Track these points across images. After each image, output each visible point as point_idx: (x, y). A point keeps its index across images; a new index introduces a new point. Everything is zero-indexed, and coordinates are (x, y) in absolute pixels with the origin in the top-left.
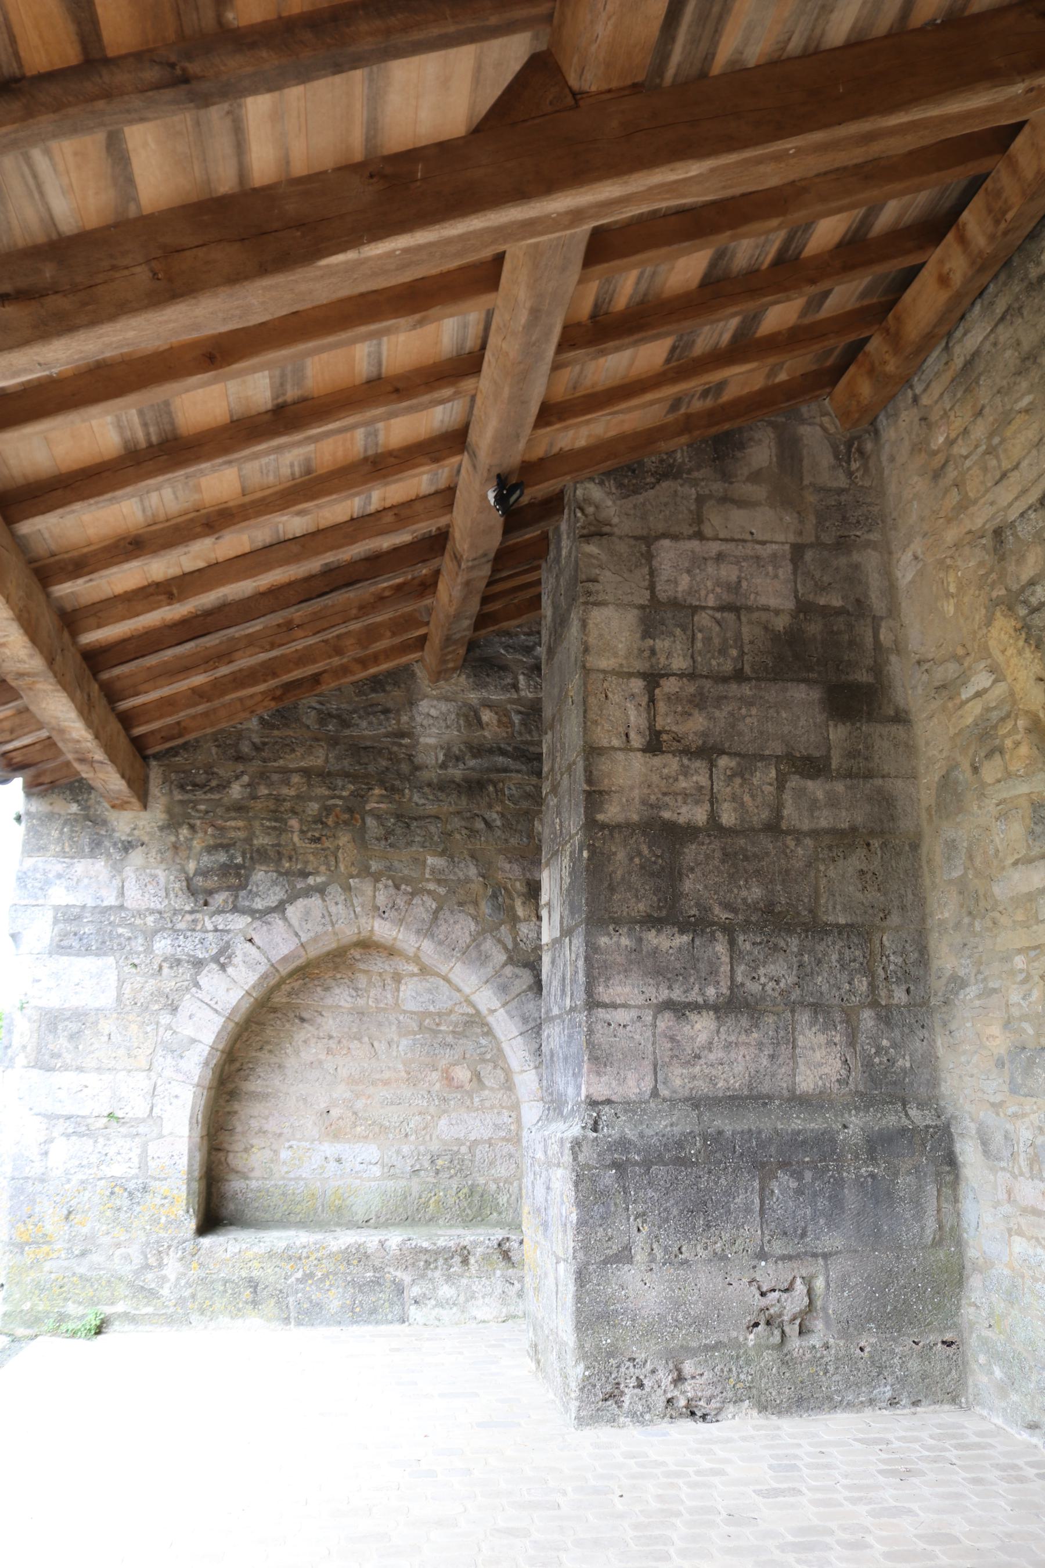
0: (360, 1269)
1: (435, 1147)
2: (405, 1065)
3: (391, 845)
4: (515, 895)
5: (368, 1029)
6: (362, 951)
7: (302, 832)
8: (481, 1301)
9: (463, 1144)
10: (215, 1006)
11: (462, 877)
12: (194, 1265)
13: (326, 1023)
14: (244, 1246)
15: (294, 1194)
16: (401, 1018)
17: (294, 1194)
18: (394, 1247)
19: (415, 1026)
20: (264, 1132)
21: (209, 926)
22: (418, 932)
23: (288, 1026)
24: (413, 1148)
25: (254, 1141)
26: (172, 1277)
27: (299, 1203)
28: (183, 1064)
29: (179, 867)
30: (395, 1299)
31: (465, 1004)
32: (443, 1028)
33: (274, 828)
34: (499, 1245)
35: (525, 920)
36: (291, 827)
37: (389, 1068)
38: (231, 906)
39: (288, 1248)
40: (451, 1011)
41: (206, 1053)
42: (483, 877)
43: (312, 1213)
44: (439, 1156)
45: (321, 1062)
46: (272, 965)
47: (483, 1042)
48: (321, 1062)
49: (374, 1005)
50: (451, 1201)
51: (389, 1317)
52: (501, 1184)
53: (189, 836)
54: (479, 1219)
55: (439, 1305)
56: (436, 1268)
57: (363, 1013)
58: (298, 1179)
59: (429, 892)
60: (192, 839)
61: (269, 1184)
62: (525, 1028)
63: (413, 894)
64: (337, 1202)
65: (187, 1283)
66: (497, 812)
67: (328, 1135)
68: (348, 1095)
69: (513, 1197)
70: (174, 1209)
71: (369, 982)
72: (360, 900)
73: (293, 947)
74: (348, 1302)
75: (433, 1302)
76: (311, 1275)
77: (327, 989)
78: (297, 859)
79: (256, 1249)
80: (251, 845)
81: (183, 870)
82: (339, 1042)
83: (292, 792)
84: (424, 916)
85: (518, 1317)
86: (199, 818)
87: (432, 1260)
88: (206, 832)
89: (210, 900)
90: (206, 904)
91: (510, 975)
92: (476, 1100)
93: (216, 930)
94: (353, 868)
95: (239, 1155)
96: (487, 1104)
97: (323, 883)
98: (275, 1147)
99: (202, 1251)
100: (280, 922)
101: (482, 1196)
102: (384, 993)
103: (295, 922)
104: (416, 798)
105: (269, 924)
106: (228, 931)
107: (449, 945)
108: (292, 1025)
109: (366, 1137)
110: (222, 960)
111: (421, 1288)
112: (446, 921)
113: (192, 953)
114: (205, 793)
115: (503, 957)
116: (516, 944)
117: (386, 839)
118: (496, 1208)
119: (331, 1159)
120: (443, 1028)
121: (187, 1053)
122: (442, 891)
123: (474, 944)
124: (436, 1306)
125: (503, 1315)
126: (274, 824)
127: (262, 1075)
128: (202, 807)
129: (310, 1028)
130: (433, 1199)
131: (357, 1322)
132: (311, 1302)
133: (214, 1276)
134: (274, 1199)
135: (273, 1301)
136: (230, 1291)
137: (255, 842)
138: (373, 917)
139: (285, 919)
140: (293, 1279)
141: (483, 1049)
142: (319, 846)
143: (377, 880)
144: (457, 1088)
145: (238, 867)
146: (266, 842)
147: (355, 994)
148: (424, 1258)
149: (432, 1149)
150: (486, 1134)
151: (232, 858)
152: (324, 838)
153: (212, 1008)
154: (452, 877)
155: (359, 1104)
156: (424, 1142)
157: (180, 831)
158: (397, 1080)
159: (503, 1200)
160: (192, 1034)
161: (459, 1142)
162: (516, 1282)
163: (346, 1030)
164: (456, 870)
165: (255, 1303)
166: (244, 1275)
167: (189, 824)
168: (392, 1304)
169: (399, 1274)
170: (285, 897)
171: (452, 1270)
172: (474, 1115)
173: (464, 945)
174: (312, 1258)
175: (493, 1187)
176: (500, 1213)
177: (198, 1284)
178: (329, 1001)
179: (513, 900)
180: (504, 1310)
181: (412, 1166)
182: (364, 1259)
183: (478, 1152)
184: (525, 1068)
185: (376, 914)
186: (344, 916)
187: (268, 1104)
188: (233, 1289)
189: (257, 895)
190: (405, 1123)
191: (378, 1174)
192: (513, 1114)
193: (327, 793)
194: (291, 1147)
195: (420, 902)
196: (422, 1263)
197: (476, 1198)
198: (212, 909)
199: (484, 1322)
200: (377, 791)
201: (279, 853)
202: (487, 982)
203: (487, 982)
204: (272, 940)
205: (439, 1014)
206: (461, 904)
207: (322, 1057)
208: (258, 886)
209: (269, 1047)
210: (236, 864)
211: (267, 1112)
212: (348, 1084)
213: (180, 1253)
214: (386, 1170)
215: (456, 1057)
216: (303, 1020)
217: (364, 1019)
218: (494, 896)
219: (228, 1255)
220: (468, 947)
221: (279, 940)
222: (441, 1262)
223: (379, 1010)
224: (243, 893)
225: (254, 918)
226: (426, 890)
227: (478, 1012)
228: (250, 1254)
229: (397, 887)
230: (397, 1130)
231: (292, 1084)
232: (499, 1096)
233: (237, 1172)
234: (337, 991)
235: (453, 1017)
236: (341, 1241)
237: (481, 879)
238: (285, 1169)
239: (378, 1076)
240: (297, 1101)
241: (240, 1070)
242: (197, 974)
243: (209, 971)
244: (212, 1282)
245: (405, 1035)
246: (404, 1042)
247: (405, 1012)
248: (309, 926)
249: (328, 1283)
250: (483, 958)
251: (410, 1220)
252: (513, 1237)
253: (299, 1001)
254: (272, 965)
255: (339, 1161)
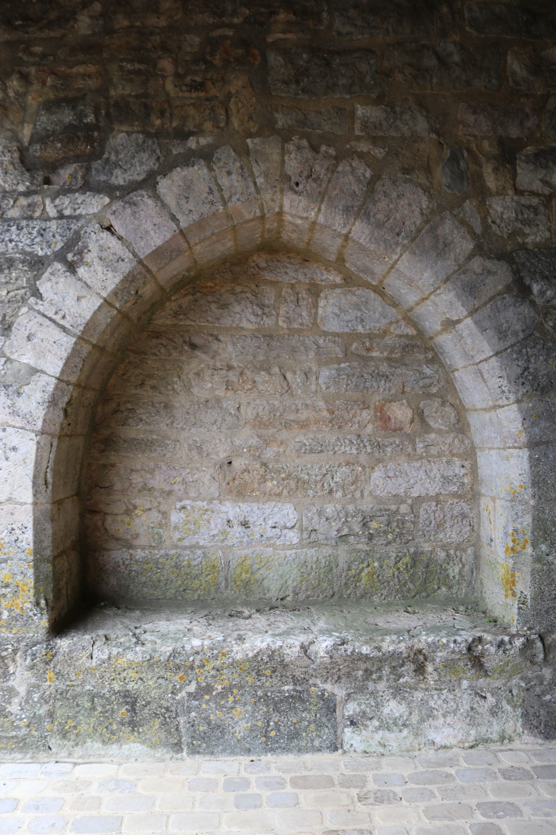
0: (275, 681)
1: (367, 505)
2: (326, 402)
3: (304, 91)
4: (483, 159)
5: (278, 356)
6: (268, 257)
7: (177, 75)
8: (442, 720)
9: (403, 502)
10: (62, 322)
11: (407, 133)
12: (50, 674)
13: (224, 350)
14: (115, 651)
15: (189, 566)
16: (321, 341)
17: (189, 566)
18: (322, 654)
19: (339, 352)
20: (150, 490)
21: (52, 212)
22: (347, 210)
23: (175, 354)
24: (339, 507)
25: (138, 501)
26: (22, 690)
27: (196, 577)
28: (22, 404)
29: (9, 134)
30: (324, 720)
31: (403, 323)
32: (374, 354)
33: (138, 72)
34: (469, 649)
35: (498, 194)
36: (163, 70)
37: (307, 405)
38: (80, 182)
39: (174, 654)
40: (385, 332)
41: (51, 388)
42: (437, 133)
43: (213, 589)
44: (372, 518)
45: (218, 400)
46: (140, 262)
47: (428, 371)
48: (218, 400)
49: (285, 326)
50: (389, 573)
51: (317, 743)
52: (452, 552)
53: (21, 90)
54: (424, 594)
55: (385, 726)
56: (380, 678)
57: (271, 337)
58: (194, 547)
59: (361, 156)
60: (25, 94)
61: (158, 554)
62: (501, 346)
63: (338, 159)
64: (244, 576)
65: (41, 697)
66: (455, 43)
67: (231, 491)
68: (254, 441)
69: (467, 568)
70: (19, 601)
71: (279, 296)
72: (263, 167)
73: (169, 236)
74: (260, 724)
75: (376, 723)
76: (208, 689)
77: (225, 306)
78: (171, 114)
79: (130, 656)
80: (107, 98)
81: (15, 137)
82: (242, 374)
83: (163, 22)
84: (355, 187)
85: (492, 741)
86: (34, 64)
87: (374, 669)
88: (44, 83)
89: (54, 178)
90: (47, 181)
91: (479, 271)
92: (420, 445)
93: (61, 216)
94: (251, 124)
95: (119, 518)
96: (433, 451)
97: (209, 145)
98: (163, 508)
99: (60, 657)
100: (150, 202)
101: (427, 566)
102: (298, 310)
103: (170, 200)
104: (338, 24)
105: (135, 204)
106: (78, 218)
107: (392, 229)
108: (181, 353)
109: (279, 495)
110: (70, 257)
111: (359, 705)
112: (386, 194)
113: (28, 249)
114: (41, 29)
115: (469, 246)
116: (486, 227)
117: (297, 82)
118: (446, 581)
119: (235, 522)
120: (374, 354)
121: (26, 388)
122: (379, 153)
123: (427, 227)
124: (378, 729)
125: (472, 738)
126: (137, 66)
127: (144, 417)
128: (38, 49)
129: (203, 356)
130: (366, 571)
131: (272, 750)
132: (209, 724)
133: (79, 689)
134: (165, 573)
135: (157, 723)
136: (99, 709)
137: (112, 93)
138: (282, 191)
139: (157, 197)
140: (183, 693)
141: (427, 381)
142: (202, 94)
143: (286, 140)
144: (395, 430)
145: (90, 128)
146: (127, 92)
147: (260, 312)
148: (363, 666)
149: (364, 508)
150: (433, 489)
151: (81, 116)
152: (209, 83)
153: (58, 325)
154: (393, 133)
155: (269, 453)
156: (353, 500)
157: (9, 83)
158: (317, 422)
159: (454, 571)
160: (32, 363)
161: (398, 499)
162: (489, 695)
163: (250, 358)
164: (398, 123)
165: (133, 725)
166: (117, 688)
167: (20, 72)
168: (320, 726)
169: (328, 687)
170: (156, 167)
171: (401, 680)
172: (417, 464)
173: (413, 228)
174: (208, 667)
175: (443, 555)
176: (450, 588)
177: (55, 699)
178: (227, 322)
179: (481, 166)
180: (473, 732)
181: (338, 531)
182: (280, 668)
183: (422, 512)
184: (500, 402)
185: (286, 186)
186: (239, 190)
187: (153, 455)
188: (103, 706)
189: (116, 165)
190: (329, 477)
191: (295, 541)
192: (467, 464)
193: (211, 20)
194: (184, 508)
195: (348, 168)
196: (360, 673)
197: (420, 570)
198: (55, 187)
199: (445, 747)
200: (282, 16)
201: (145, 106)
202: (447, 279)
203: (447, 279)
204: (139, 226)
205: (370, 336)
206: (406, 171)
207: (221, 393)
208: (117, 153)
209: (153, 382)
210: (87, 124)
211: (152, 465)
212: (254, 427)
213: (29, 659)
214: (305, 536)
215: (393, 391)
216: (194, 347)
217: (274, 343)
218: (454, 159)
219: (94, 663)
220: (419, 231)
221: (148, 226)
222: (386, 670)
223: (292, 332)
224: (97, 164)
225: (113, 198)
226: (356, 152)
227: (421, 333)
228: (122, 662)
229: (315, 149)
230: (319, 486)
231: (183, 429)
232: (449, 441)
233: (118, 539)
234: (238, 308)
235: (388, 340)
236: (247, 645)
237: (434, 136)
238: (177, 535)
239: (292, 417)
240: (190, 450)
241: (116, 411)
242: (37, 277)
243: (52, 274)
244: (75, 697)
245: (326, 364)
246: (325, 373)
247: (325, 334)
248: (191, 206)
249: (231, 699)
250: (441, 246)
251: (336, 597)
252: (488, 637)
253: (188, 322)
254: (140, 262)
255: (245, 524)
